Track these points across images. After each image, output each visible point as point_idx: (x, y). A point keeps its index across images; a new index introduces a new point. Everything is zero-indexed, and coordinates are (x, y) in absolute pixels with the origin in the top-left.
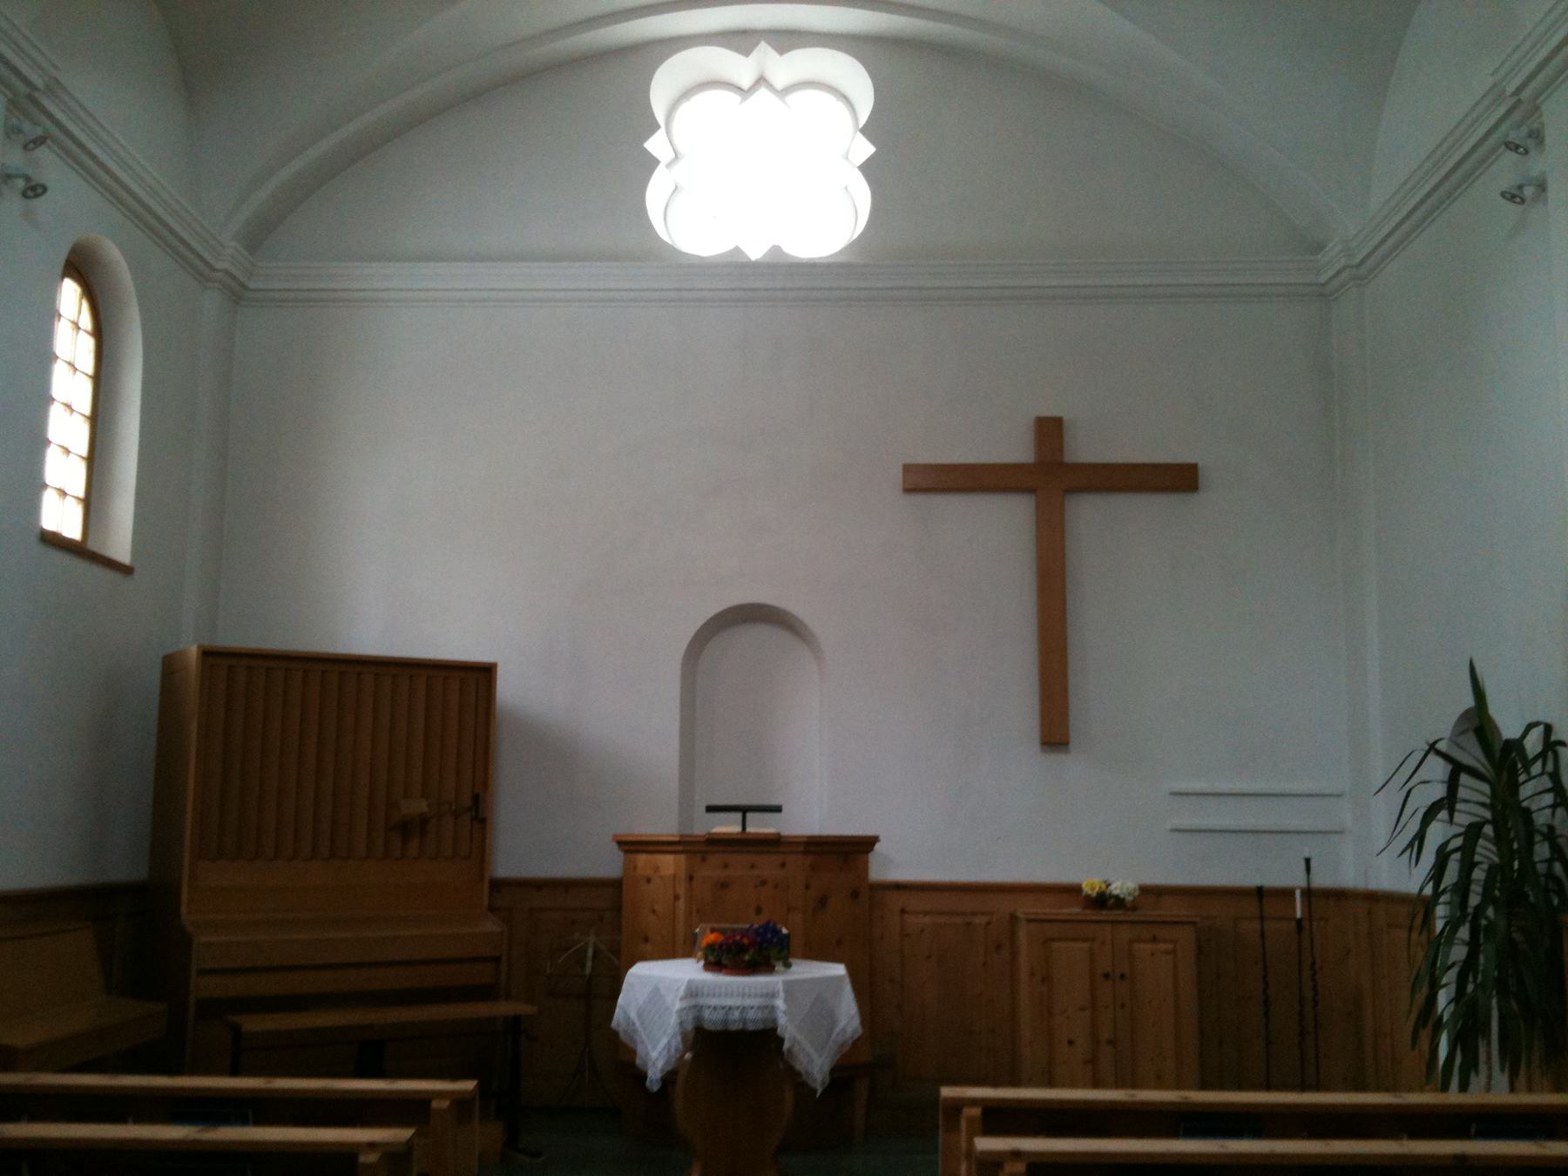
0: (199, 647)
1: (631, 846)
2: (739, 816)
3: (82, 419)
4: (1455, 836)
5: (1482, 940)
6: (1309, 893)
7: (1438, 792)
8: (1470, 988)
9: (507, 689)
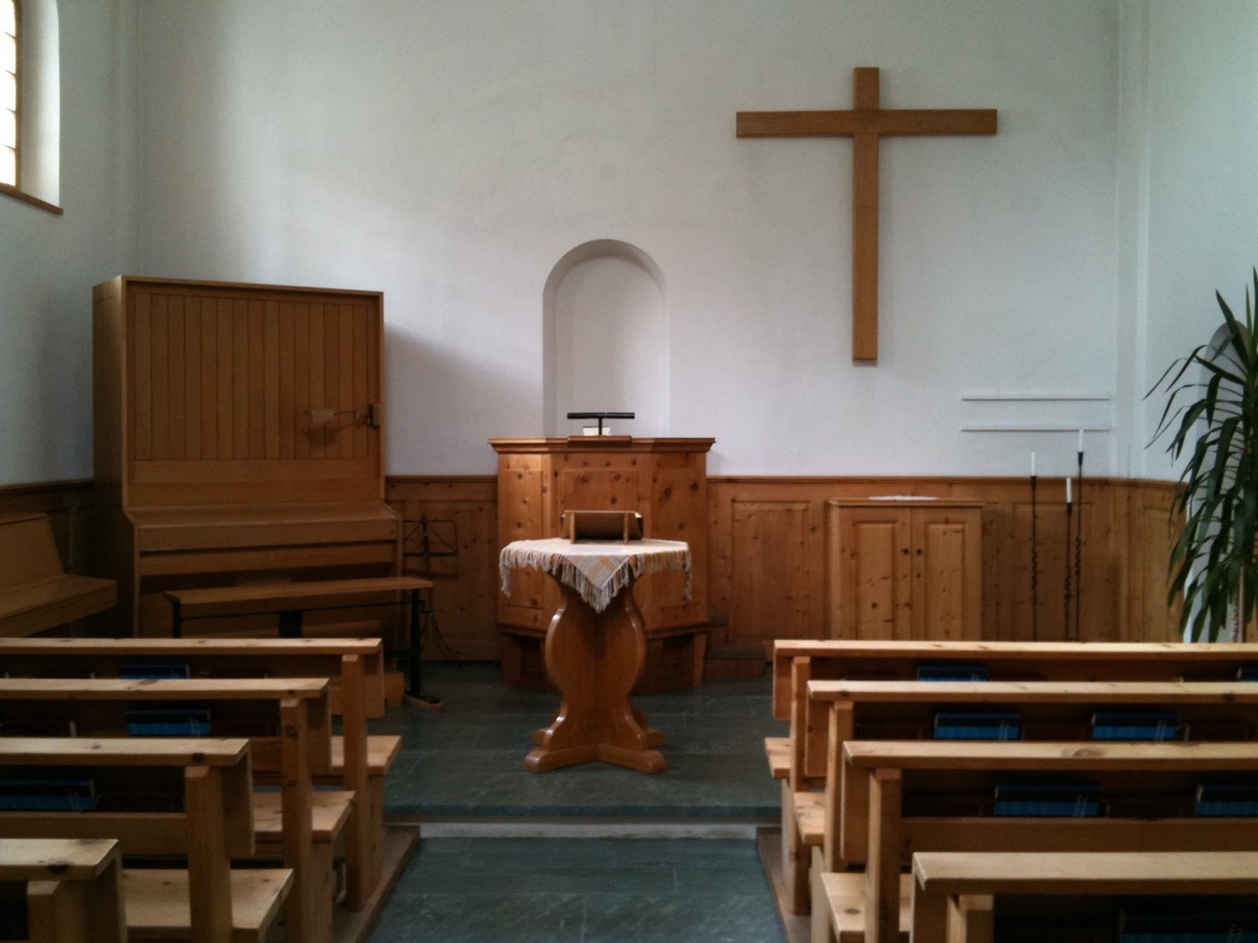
0: (123, 277)
1: (504, 449)
2: (596, 421)
3: (11, 76)
4: (1214, 430)
5: (1233, 518)
6: (1079, 482)
7: (1196, 395)
8: (1222, 557)
9: (394, 316)
